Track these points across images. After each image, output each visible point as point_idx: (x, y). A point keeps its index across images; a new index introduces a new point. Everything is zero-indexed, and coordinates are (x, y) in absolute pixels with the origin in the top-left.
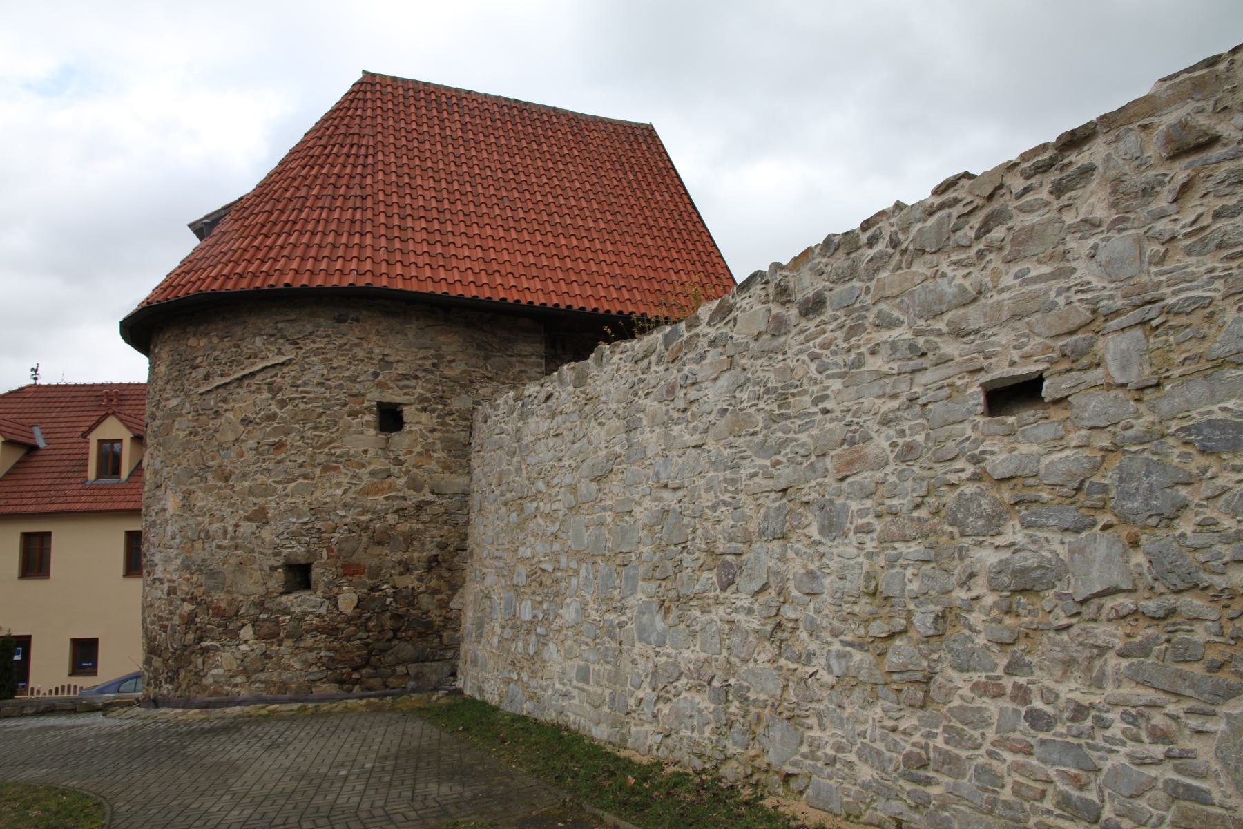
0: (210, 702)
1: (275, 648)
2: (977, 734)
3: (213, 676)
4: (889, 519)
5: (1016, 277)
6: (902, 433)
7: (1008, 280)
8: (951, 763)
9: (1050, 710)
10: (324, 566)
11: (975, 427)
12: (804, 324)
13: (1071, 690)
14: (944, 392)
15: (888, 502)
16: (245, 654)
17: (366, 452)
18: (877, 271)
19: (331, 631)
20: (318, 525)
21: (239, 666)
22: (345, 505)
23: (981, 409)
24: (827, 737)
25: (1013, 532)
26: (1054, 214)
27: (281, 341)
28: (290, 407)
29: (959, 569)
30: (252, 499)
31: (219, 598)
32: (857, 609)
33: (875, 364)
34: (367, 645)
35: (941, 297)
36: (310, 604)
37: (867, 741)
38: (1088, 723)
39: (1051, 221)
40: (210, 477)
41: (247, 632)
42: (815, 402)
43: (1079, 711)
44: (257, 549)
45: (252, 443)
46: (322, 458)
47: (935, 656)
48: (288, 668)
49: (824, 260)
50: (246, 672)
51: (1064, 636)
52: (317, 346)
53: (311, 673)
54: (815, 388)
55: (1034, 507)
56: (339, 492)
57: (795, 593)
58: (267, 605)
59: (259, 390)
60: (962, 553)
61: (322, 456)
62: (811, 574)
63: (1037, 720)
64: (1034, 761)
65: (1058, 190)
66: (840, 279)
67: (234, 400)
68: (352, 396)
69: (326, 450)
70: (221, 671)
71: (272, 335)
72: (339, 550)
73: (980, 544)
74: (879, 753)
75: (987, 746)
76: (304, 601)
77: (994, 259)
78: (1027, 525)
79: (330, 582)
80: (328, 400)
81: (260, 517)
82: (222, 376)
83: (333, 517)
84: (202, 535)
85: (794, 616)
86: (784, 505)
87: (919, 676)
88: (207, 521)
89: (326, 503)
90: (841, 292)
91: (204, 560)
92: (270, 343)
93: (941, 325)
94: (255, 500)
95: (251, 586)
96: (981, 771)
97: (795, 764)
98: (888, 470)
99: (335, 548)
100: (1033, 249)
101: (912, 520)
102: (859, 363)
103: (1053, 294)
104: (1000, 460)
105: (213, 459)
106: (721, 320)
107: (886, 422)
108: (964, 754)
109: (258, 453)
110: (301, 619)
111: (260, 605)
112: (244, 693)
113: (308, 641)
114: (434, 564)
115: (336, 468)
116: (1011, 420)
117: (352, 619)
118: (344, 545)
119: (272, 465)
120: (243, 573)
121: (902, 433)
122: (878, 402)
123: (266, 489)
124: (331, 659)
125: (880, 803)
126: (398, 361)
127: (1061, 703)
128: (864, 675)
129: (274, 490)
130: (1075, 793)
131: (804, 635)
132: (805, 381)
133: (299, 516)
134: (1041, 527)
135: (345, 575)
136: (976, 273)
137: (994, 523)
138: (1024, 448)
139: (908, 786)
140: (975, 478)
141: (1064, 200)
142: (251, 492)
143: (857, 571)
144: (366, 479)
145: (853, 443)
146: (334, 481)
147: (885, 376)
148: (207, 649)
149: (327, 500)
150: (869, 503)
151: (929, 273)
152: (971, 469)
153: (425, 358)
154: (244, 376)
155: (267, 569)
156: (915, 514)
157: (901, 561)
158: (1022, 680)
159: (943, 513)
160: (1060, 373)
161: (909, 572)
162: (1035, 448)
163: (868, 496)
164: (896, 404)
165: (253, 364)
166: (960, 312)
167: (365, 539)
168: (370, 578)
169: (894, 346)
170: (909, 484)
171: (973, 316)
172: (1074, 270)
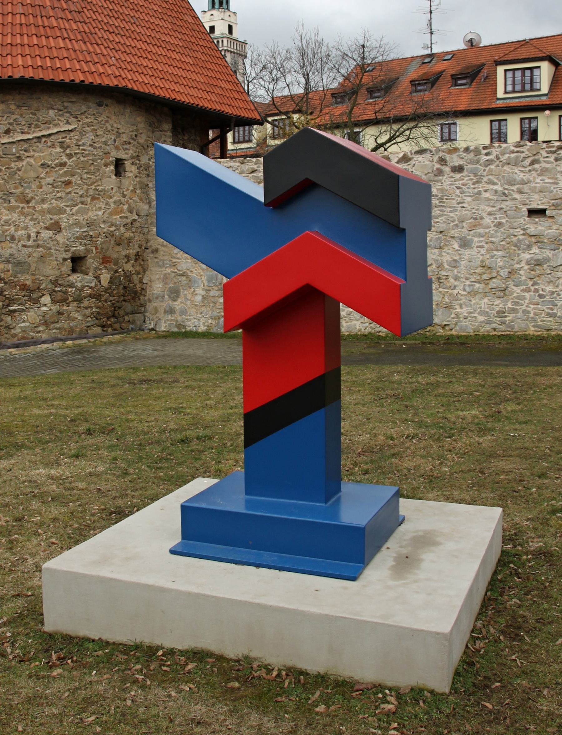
0: (20, 344)
1: (65, 308)
2: (523, 302)
3: (21, 328)
4: (491, 244)
5: (541, 180)
6: (496, 218)
7: (538, 180)
8: (514, 311)
9: (544, 293)
10: (93, 258)
11: (524, 220)
12: (452, 174)
13: (549, 288)
14: (514, 208)
15: (490, 239)
16: (45, 312)
17: (112, 189)
18: (489, 165)
19: (97, 296)
20: (91, 233)
21: (41, 320)
22: (104, 222)
23: (527, 215)
24: (464, 311)
25: (535, 249)
26: (554, 166)
27: (68, 115)
28: (74, 159)
29: (516, 259)
30: (49, 216)
31: (26, 279)
32: (476, 271)
33: (487, 195)
34: (113, 304)
35: (515, 180)
36: (86, 281)
37: (482, 309)
38: (555, 295)
39: (553, 168)
40: (12, 200)
41: (46, 299)
42: (458, 203)
43: (553, 293)
44: (53, 247)
45: (50, 180)
46: (91, 192)
47: (508, 283)
48: (74, 319)
49: (465, 154)
50: (46, 324)
51: (549, 276)
52: (89, 120)
53: (87, 322)
54: (459, 199)
55: (542, 244)
56: (100, 213)
57: (447, 267)
58: (60, 282)
59: (53, 146)
60: (519, 255)
61: (91, 191)
62: (455, 261)
63: (541, 296)
64: (539, 306)
65: (556, 160)
66: (471, 163)
67: (34, 151)
68: (105, 153)
69: (93, 187)
70: (27, 324)
71: (60, 110)
72: (102, 248)
73: (524, 253)
74: (487, 312)
75: (526, 304)
76: (83, 279)
77: (534, 174)
78: (539, 248)
79: (97, 268)
80: (95, 156)
81: (56, 227)
82: (22, 133)
83: (98, 228)
84: (8, 238)
85: (447, 274)
86: (441, 237)
87: (502, 289)
88: (13, 229)
89: (95, 220)
90: (471, 168)
91: (11, 255)
92: (60, 116)
93: (515, 188)
94: (51, 217)
95: (50, 270)
96: (524, 311)
97: (449, 321)
98: (491, 229)
99: (99, 247)
100: (547, 174)
101: (500, 245)
102: (479, 193)
103: (552, 188)
104: (532, 229)
105: (16, 188)
106: (405, 163)
107: (490, 214)
108: (518, 307)
109: (53, 187)
110: (81, 290)
111: (55, 283)
112: (45, 336)
113: (86, 303)
114: (137, 257)
115: (98, 198)
116: (537, 220)
117: (108, 289)
118: (103, 246)
119: (63, 194)
120: (44, 262)
121: (496, 218)
122: (487, 208)
123: (59, 210)
124: (98, 313)
125: (488, 326)
126: (124, 133)
127: (547, 292)
128: (481, 290)
129: (65, 211)
130: (551, 311)
131: (452, 280)
132: (454, 195)
133: (81, 228)
134: (544, 249)
135: (103, 263)
136: (527, 176)
137: (529, 247)
138: (540, 228)
139: (498, 319)
140: (523, 234)
141: (558, 163)
142: (49, 212)
143: (477, 259)
144: (112, 205)
145: (476, 219)
146: (97, 206)
147: (491, 200)
148: (14, 311)
149: (95, 218)
150: (482, 239)
151: (511, 171)
152: (522, 232)
153: (132, 131)
154: (43, 136)
155: (61, 260)
156: (501, 243)
157: (496, 257)
158: (536, 287)
159: (512, 243)
160: (552, 210)
161: (499, 260)
162: (543, 228)
163: (482, 237)
164: (494, 209)
165: (49, 128)
166: (521, 186)
167: (112, 242)
168: (115, 265)
169: (496, 191)
170: (499, 234)
171: (526, 188)
172: (559, 183)
